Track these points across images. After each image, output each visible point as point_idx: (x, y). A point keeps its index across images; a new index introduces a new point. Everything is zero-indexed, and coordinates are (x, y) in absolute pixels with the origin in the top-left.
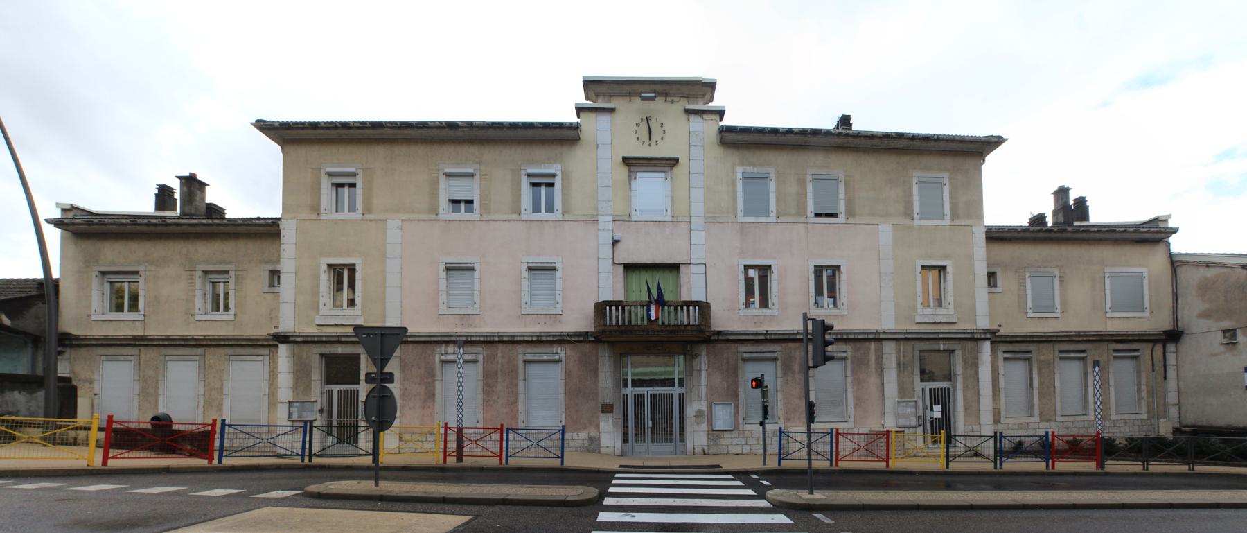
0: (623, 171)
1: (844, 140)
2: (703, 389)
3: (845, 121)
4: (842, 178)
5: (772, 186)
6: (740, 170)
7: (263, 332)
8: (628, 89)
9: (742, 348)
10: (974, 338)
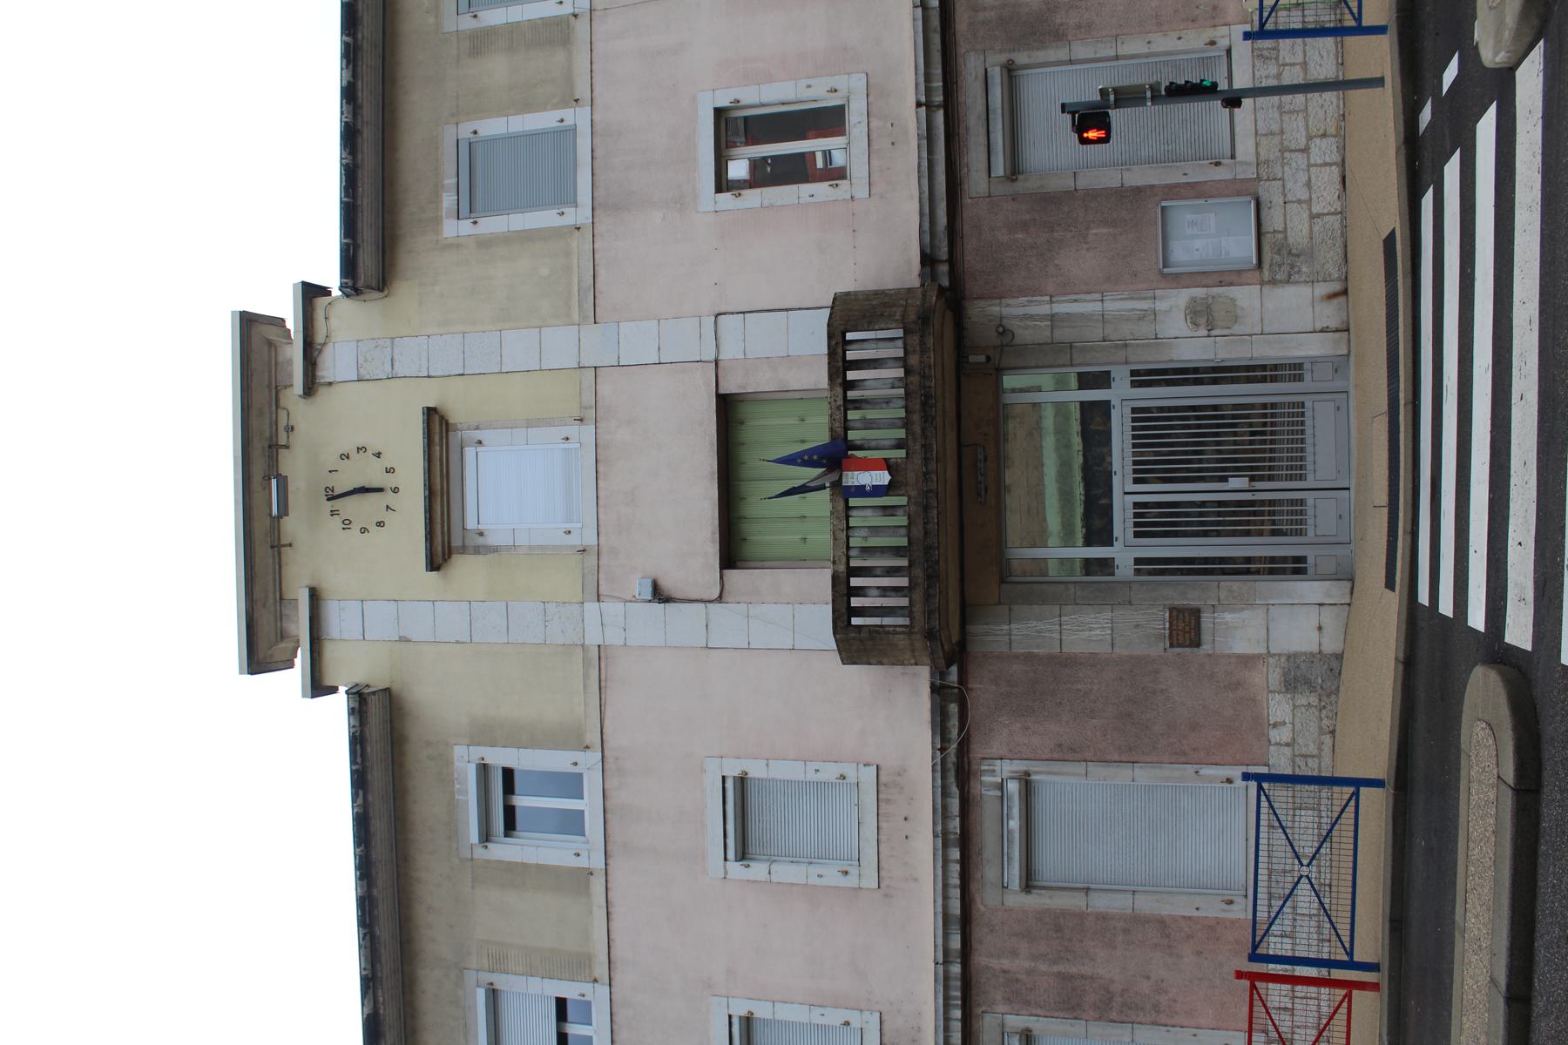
0: (464, 568)
2: (1114, 306)
6: (451, 229)
9: (976, 182)
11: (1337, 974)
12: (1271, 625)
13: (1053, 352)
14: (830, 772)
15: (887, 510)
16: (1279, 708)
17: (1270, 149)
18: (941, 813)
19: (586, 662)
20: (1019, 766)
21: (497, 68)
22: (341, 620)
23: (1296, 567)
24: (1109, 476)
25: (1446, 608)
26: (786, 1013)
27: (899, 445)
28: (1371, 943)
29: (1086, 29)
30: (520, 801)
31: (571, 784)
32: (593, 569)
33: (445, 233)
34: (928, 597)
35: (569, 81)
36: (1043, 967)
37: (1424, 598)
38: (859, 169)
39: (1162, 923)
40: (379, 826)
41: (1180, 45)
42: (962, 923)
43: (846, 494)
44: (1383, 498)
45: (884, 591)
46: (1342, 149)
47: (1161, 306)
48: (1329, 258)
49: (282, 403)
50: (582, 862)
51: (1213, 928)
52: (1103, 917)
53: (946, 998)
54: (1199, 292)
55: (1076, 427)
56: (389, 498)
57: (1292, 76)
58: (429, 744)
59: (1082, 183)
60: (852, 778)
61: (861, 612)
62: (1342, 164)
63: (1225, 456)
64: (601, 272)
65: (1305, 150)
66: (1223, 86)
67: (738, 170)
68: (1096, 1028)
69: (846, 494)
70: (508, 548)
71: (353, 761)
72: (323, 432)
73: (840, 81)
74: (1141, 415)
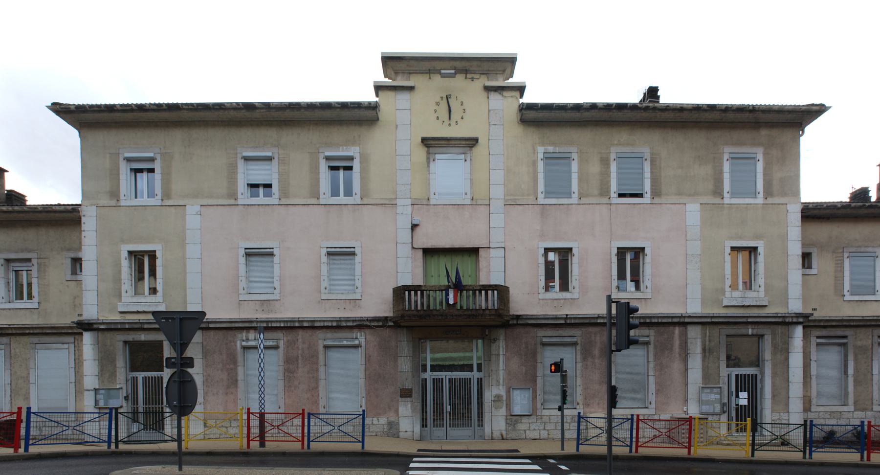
0: (422, 152)
2: (501, 374)
4: (647, 156)
6: (541, 150)
7: (67, 320)
9: (541, 333)
10: (785, 323)
11: (306, 438)
12: (407, 418)
13: (488, 356)
14: (358, 283)
15: (441, 303)
16: (383, 420)
17: (545, 419)
18: (347, 320)
19: (391, 199)
20: (363, 344)
21: (595, 168)
22: (403, 99)
23: (424, 425)
24: (452, 371)
25: (412, 465)
26: (276, 268)
27: (461, 307)
28: (315, 447)
29: (586, 367)
30: (341, 172)
31: (349, 193)
32: (421, 203)
33: (539, 145)
34: (414, 316)
35: (587, 196)
36: (300, 352)
37: (415, 459)
38: (549, 295)
39: (317, 387)
40: (328, 114)
41: (578, 394)
42: (313, 326)
43: (447, 289)
44: (444, 448)
45: (416, 302)
46: (544, 439)
47: (501, 387)
48: (513, 435)
49: (482, 76)
50: (322, 196)
51: (316, 403)
52: (317, 370)
53: (287, 322)
54: (504, 398)
55: (466, 363)
56: (447, 122)
57: (566, 426)
58: (359, 136)
59: (539, 365)
60: (357, 291)
61: (410, 294)
62: (540, 439)
63: (455, 406)
64: (521, 207)
65: (544, 429)
66: (565, 406)
67: (552, 256)
68: (282, 368)
69: (447, 289)
70: (429, 171)
71: (352, 103)
72: (469, 91)
73: (577, 290)
74: (469, 381)
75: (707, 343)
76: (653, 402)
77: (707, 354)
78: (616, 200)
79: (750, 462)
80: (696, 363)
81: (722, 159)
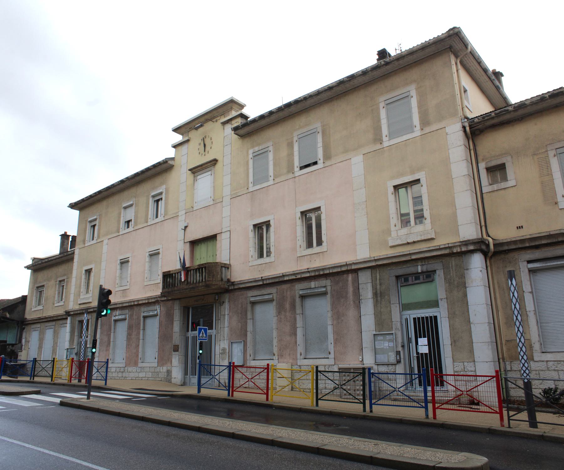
0: (191, 176)
1: (390, 67)
2: (226, 329)
3: (383, 54)
4: (320, 130)
5: (271, 156)
6: (251, 151)
7: (61, 312)
8: (220, 110)
9: (251, 293)
10: (457, 254)
23: (186, 373)
26: (160, 260)
28: (237, 395)
29: (280, 321)
32: (190, 211)
41: (274, 346)
54: (227, 351)
75: (378, 287)
76: (332, 352)
77: (379, 298)
78: (298, 172)
79: (364, 418)
80: (368, 308)
81: (378, 109)
